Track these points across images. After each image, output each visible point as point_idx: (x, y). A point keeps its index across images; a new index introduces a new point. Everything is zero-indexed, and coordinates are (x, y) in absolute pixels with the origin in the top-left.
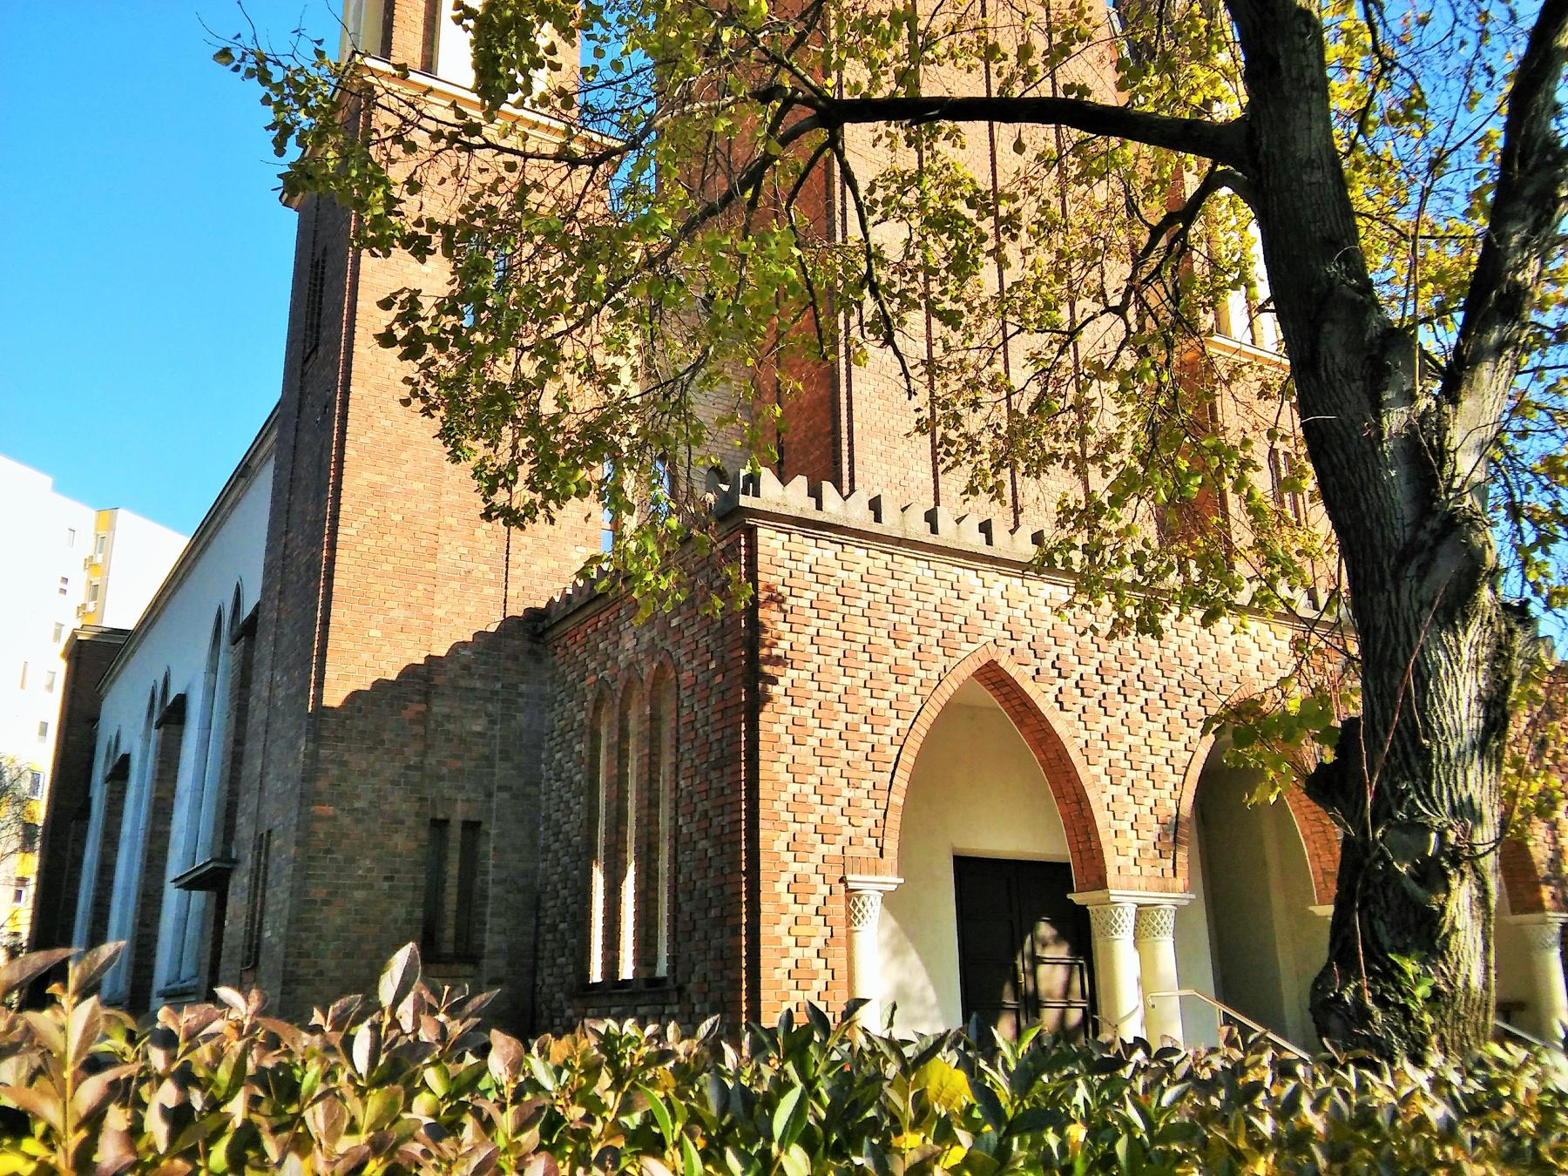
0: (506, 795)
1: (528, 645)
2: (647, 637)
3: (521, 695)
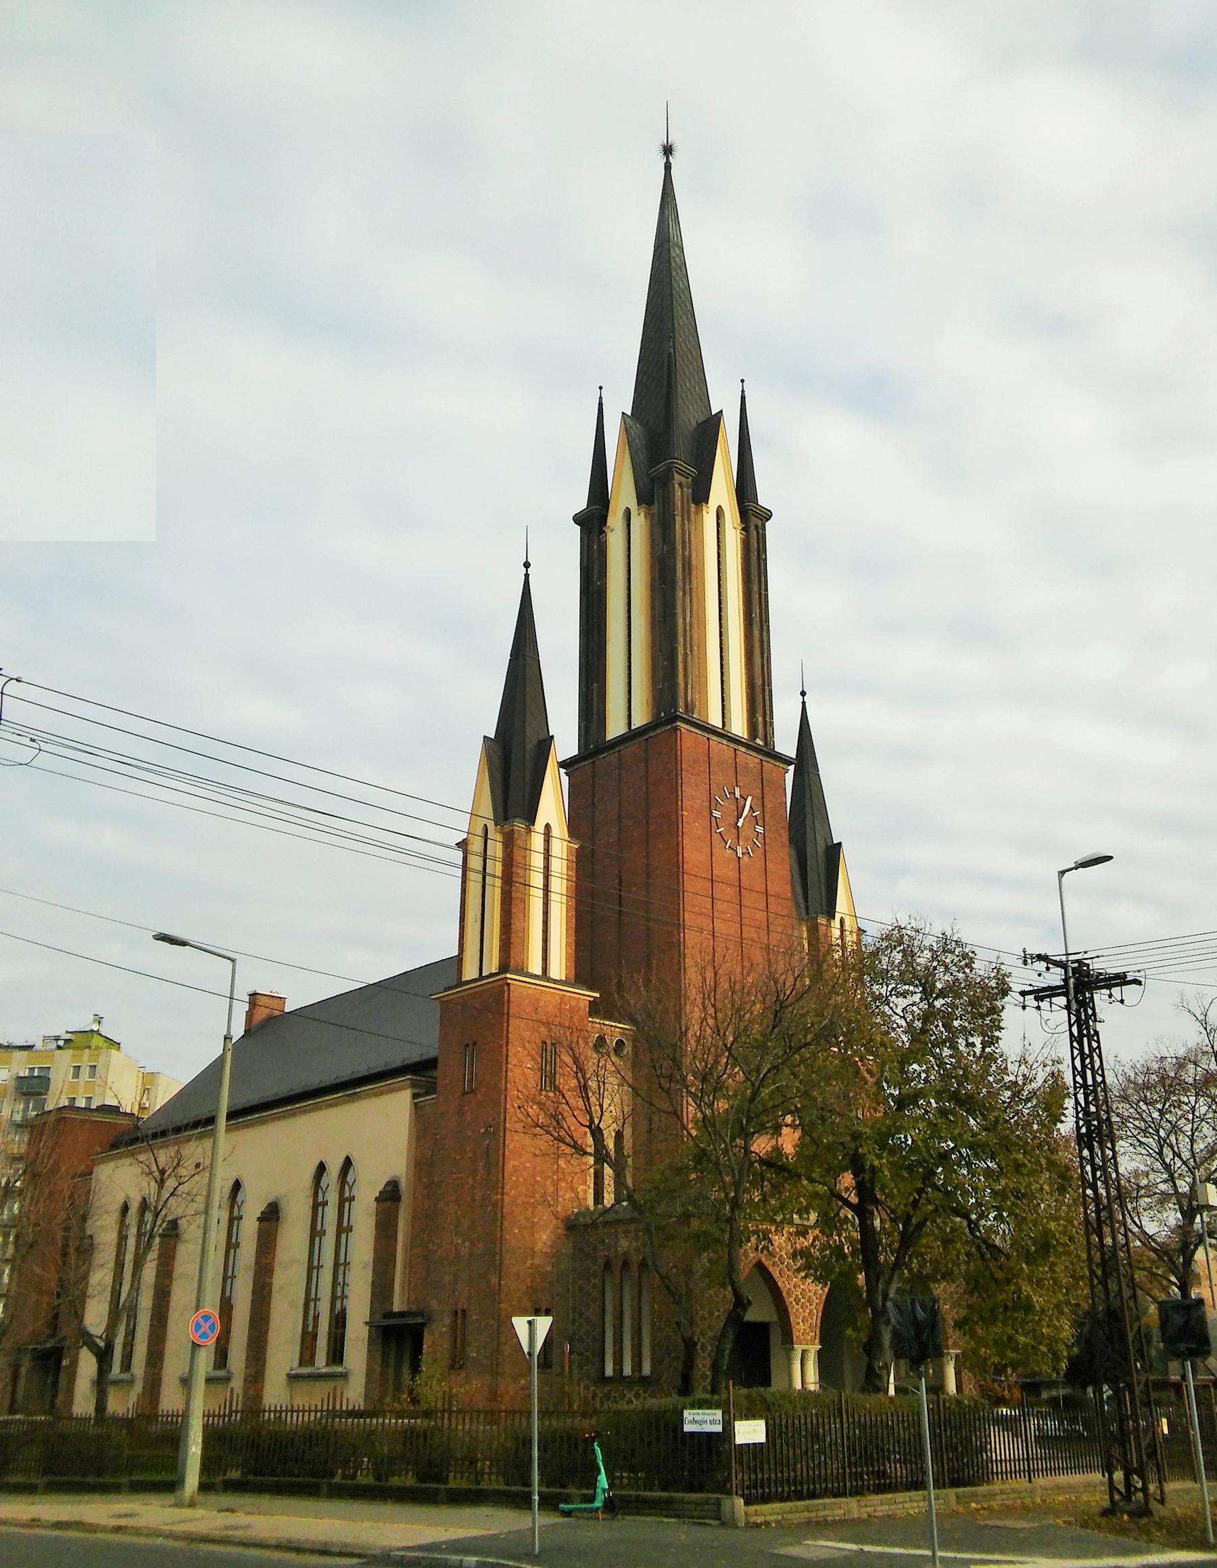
0: (558, 1298)
1: (565, 1232)
2: (634, 1244)
3: (562, 1254)
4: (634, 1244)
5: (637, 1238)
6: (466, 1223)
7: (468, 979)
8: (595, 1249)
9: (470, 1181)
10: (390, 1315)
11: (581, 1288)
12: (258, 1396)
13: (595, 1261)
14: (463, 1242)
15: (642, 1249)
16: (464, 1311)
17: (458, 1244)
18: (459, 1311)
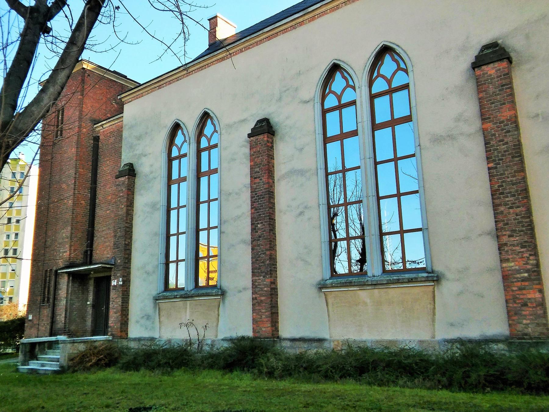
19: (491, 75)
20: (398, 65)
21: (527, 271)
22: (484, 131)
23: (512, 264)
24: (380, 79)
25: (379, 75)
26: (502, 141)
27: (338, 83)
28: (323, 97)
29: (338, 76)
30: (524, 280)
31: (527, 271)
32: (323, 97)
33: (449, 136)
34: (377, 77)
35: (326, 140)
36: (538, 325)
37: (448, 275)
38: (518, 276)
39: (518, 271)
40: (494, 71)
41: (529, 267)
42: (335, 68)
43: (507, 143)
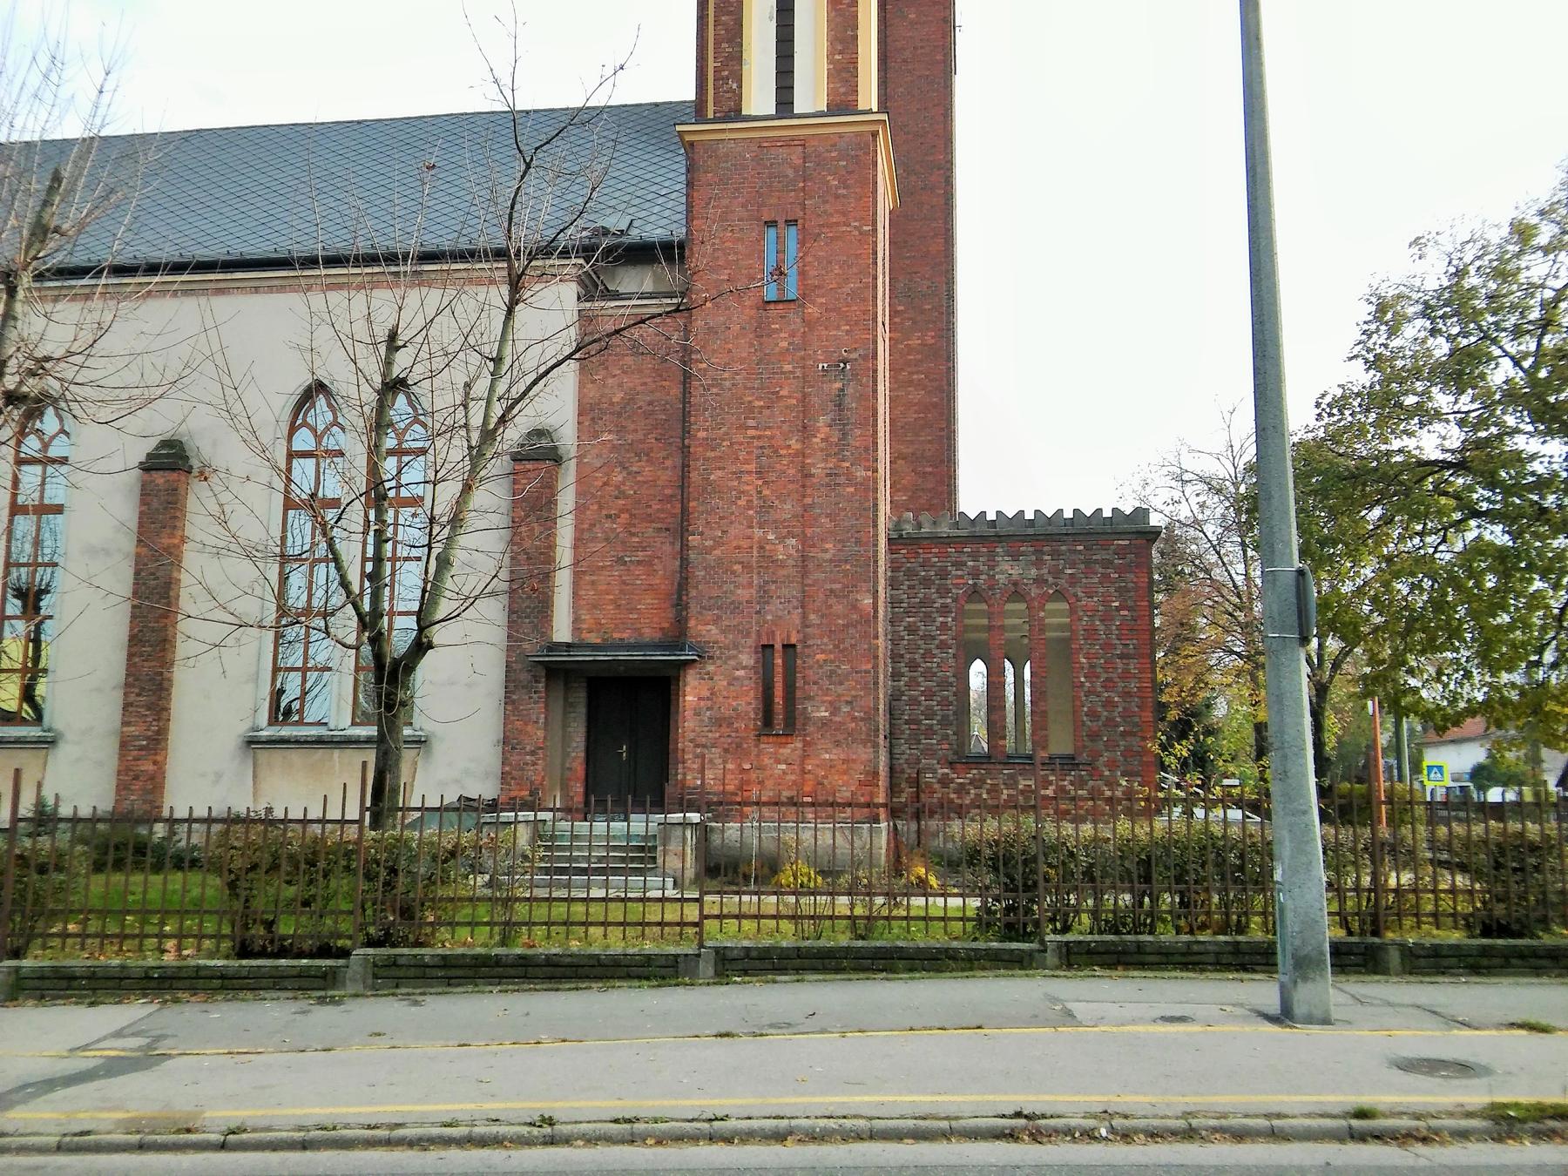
2: (1034, 572)
4: (1034, 572)
5: (1039, 563)
6: (787, 509)
7: (754, 113)
8: (943, 574)
9: (795, 444)
10: (554, 647)
11: (911, 630)
12: (155, 784)
13: (943, 592)
14: (781, 539)
15: (1050, 579)
16: (789, 647)
17: (768, 542)
18: (778, 646)
19: (158, 485)
20: (335, 417)
21: (147, 738)
22: (138, 555)
23: (133, 729)
24: (304, 430)
25: (305, 424)
26: (153, 574)
27: (321, 412)
28: (293, 429)
29: (321, 402)
30: (141, 748)
31: (147, 738)
32: (293, 429)
33: (103, 549)
34: (301, 426)
35: (16, 509)
36: (145, 802)
37: (69, 736)
38: (137, 743)
39: (137, 738)
40: (162, 480)
41: (150, 733)
42: (318, 388)
43: (157, 578)
